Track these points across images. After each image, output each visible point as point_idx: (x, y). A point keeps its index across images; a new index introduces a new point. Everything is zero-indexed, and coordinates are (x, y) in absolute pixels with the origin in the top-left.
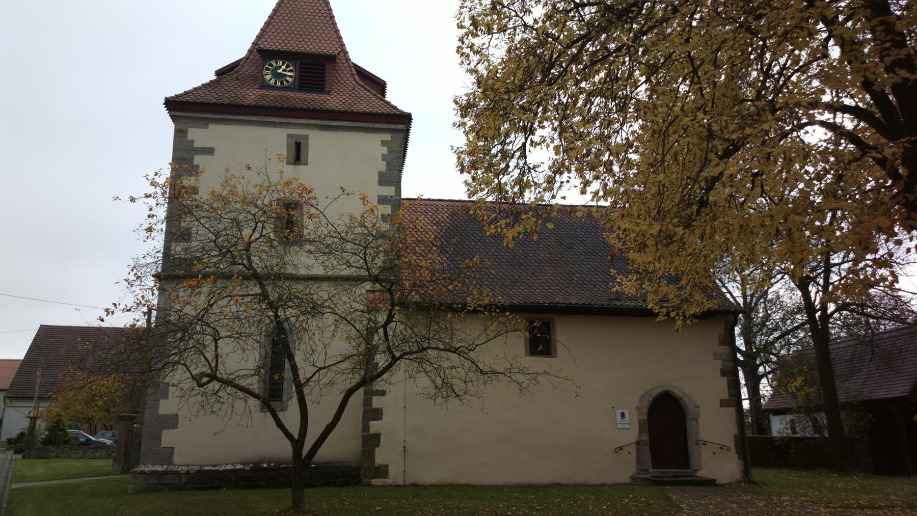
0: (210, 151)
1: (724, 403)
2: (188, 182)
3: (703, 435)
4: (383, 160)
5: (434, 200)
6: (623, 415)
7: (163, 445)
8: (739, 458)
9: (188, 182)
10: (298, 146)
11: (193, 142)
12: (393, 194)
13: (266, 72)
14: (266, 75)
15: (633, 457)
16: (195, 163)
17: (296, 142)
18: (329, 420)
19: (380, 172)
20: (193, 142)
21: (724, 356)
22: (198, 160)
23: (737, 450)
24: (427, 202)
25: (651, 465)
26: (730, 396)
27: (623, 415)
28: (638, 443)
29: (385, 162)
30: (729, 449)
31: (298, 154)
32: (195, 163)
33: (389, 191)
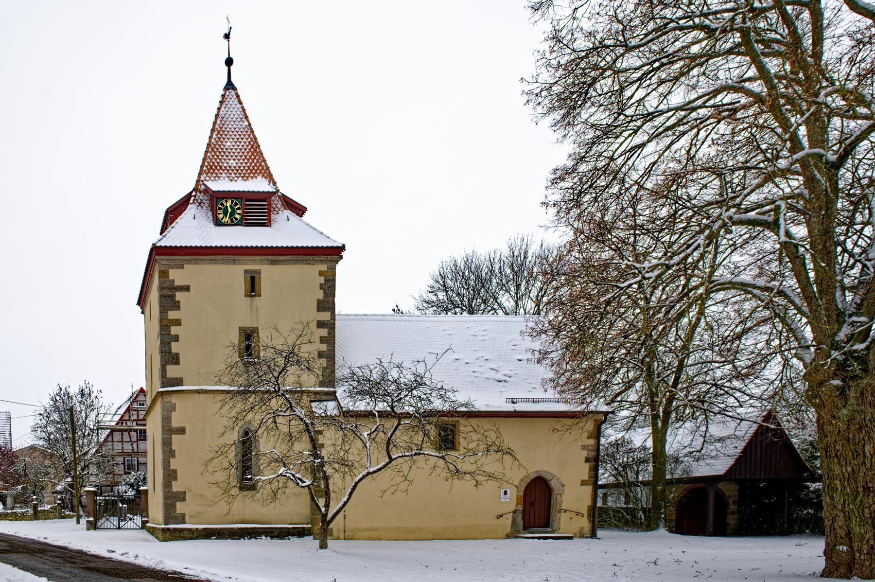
0: (187, 289)
3: (564, 506)
4: (321, 289)
5: (350, 315)
6: (505, 493)
7: (178, 512)
8: (590, 522)
9: (172, 315)
10: (253, 279)
11: (173, 281)
12: (329, 319)
13: (219, 212)
15: (510, 522)
17: (251, 277)
18: (264, 540)
19: (318, 300)
21: (589, 447)
22: (179, 296)
23: (589, 515)
24: (346, 317)
25: (522, 528)
26: (589, 477)
27: (505, 493)
28: (514, 512)
29: (322, 291)
30: (583, 516)
33: (325, 316)
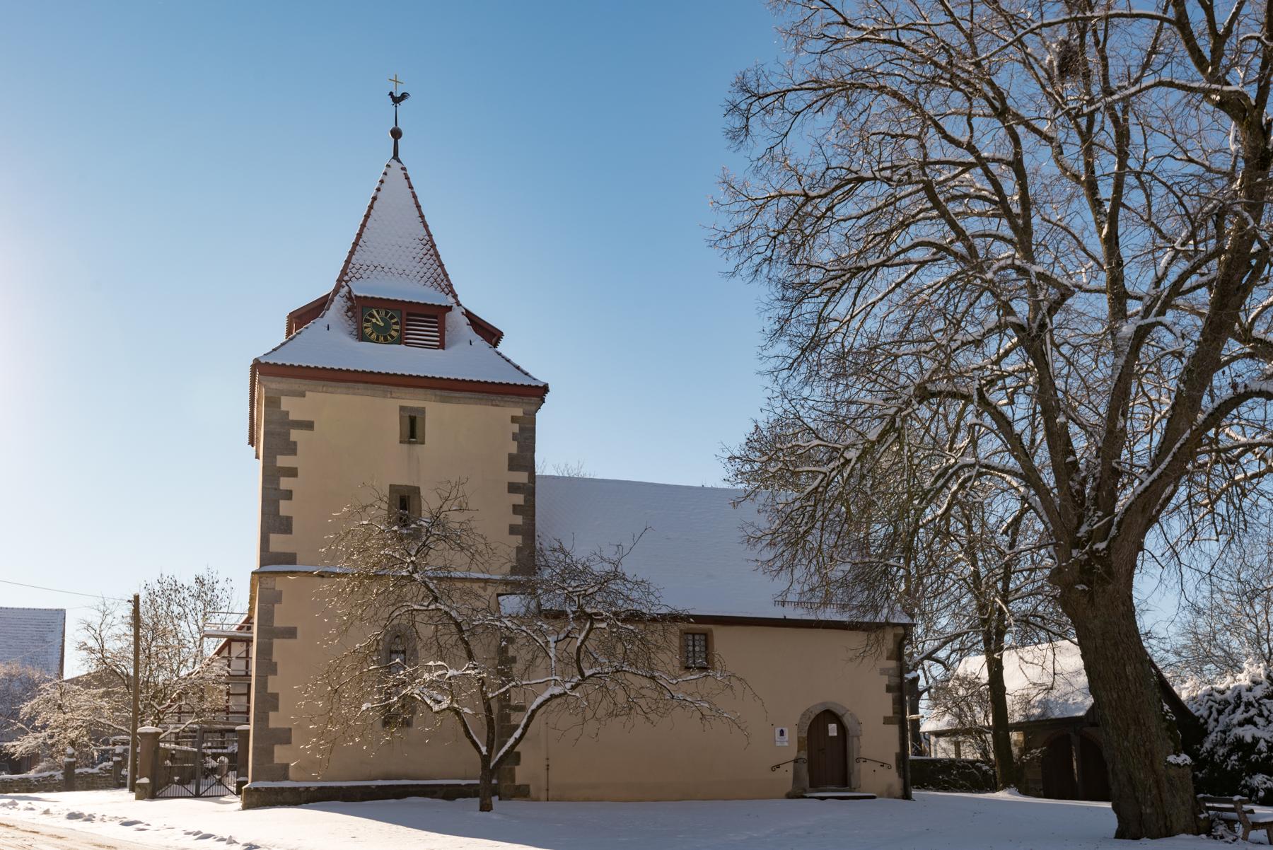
1: (887, 721)
2: (283, 461)
4: (513, 440)
6: (782, 733)
7: (276, 761)
9: (283, 461)
10: (413, 421)
11: (287, 413)
13: (366, 324)
14: (366, 328)
16: (292, 439)
17: (410, 416)
20: (287, 413)
23: (898, 767)
27: (782, 733)
31: (412, 429)
32: (292, 439)
